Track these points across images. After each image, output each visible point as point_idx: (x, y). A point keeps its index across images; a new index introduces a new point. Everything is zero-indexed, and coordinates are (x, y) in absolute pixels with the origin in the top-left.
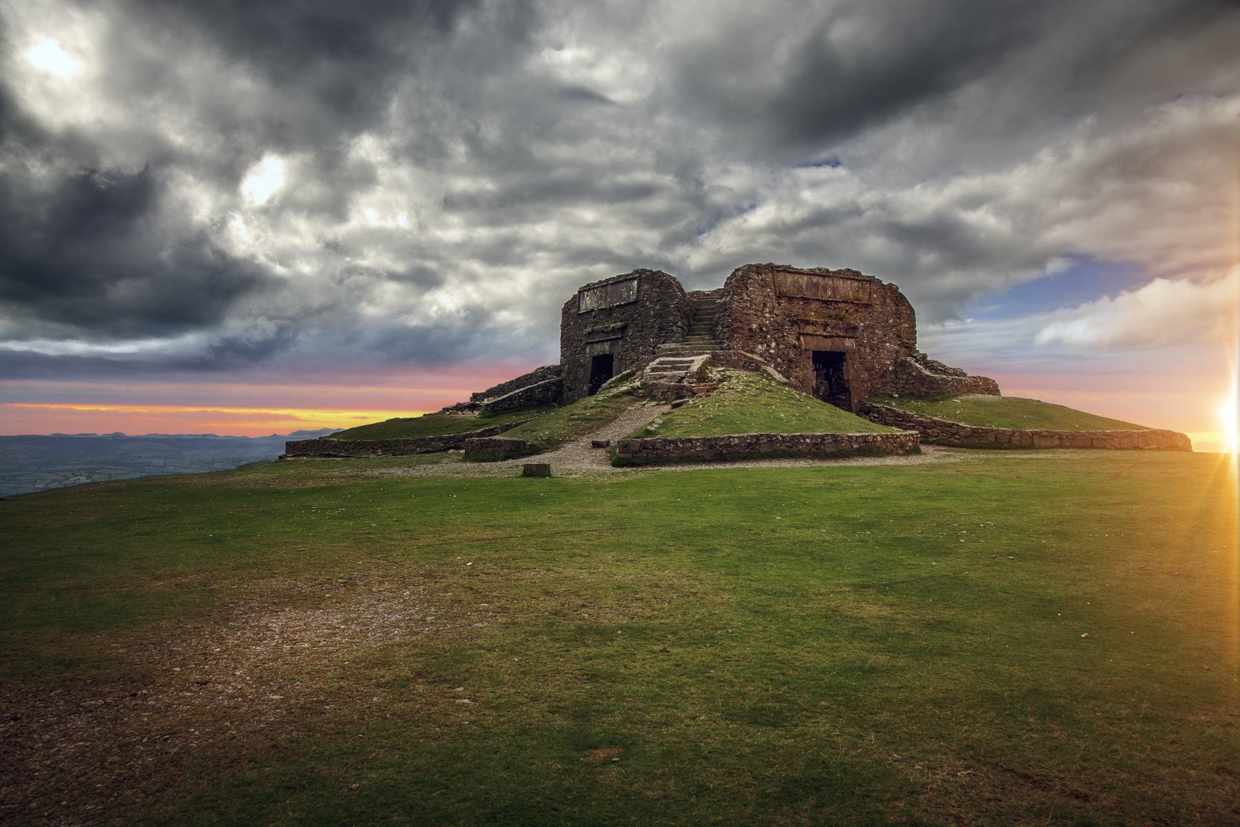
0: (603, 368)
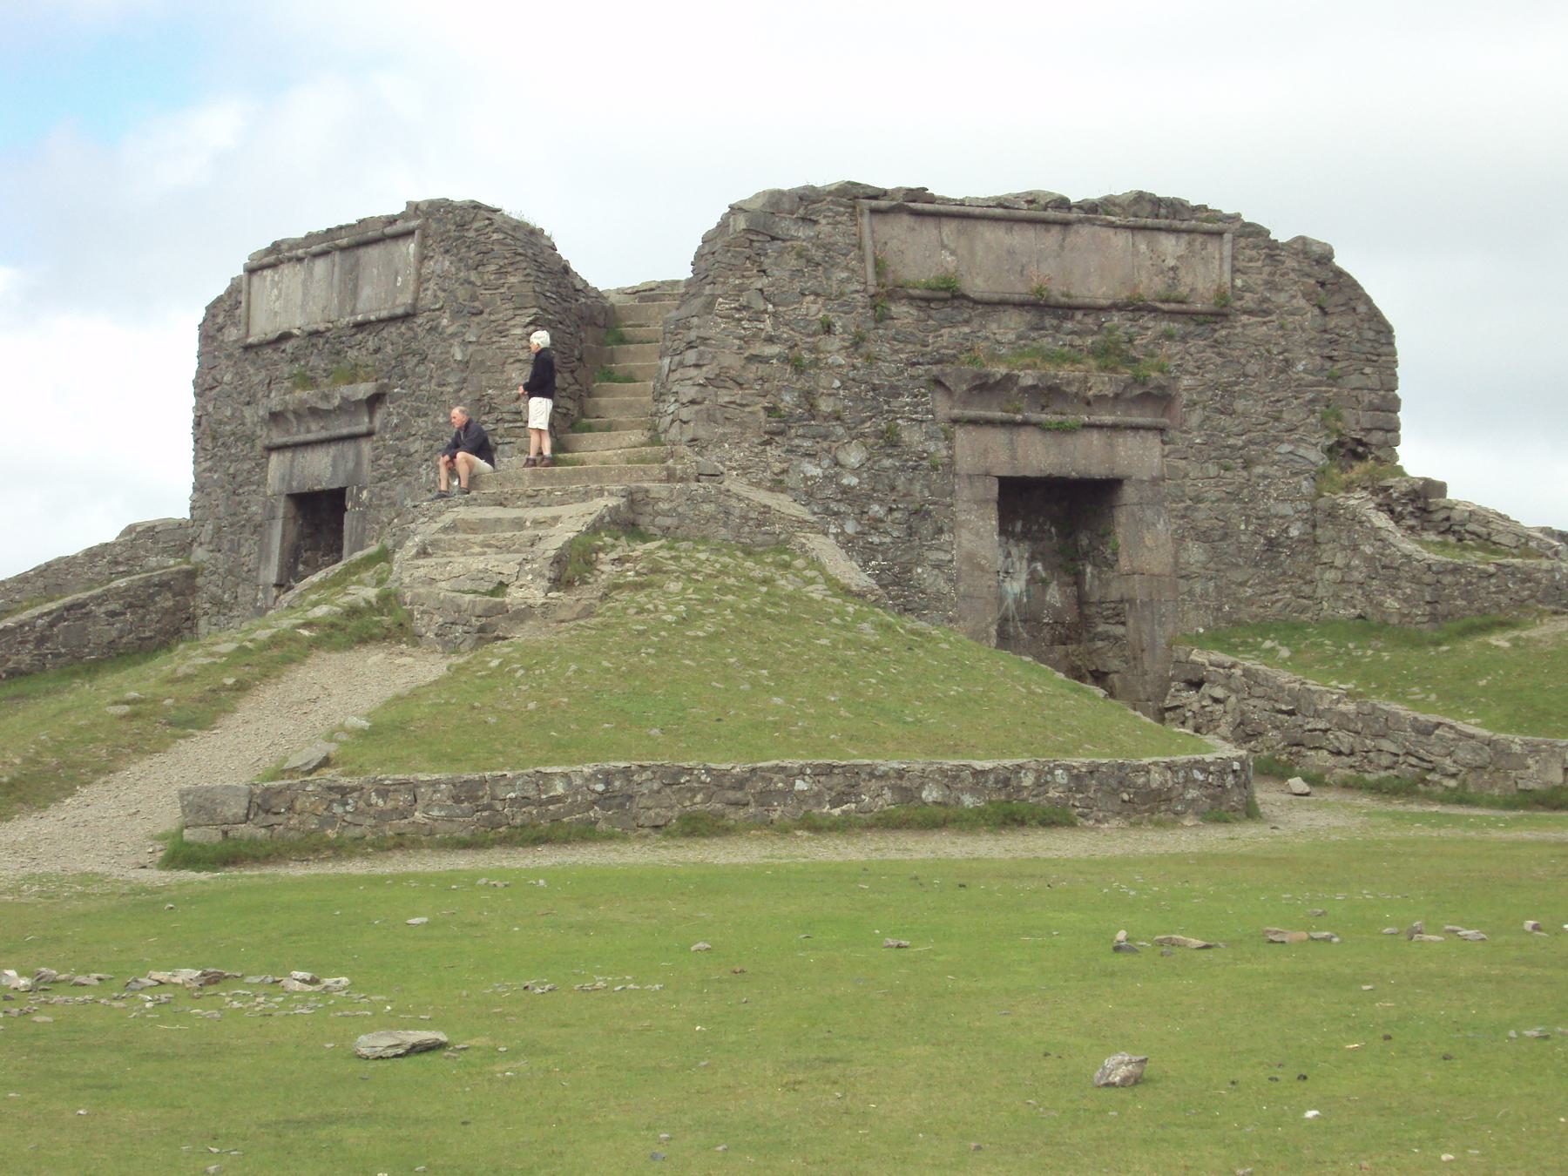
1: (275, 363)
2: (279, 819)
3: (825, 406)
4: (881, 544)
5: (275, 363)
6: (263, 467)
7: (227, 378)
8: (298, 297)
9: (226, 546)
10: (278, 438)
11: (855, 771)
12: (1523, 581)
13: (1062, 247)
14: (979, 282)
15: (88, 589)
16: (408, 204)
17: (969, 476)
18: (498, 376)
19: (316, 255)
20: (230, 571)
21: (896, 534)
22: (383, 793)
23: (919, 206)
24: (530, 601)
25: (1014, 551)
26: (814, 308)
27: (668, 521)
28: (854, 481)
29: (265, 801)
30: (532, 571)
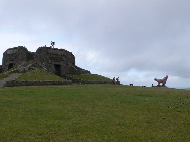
0: (11, 66)
3: (44, 59)
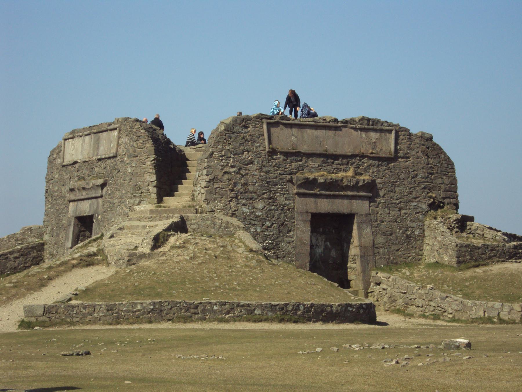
1: (72, 172)
2: (54, 315)
4: (269, 235)
5: (72, 172)
6: (67, 207)
7: (57, 176)
8: (80, 149)
9: (55, 234)
10: (73, 197)
11: (233, 304)
12: (492, 250)
13: (335, 135)
14: (305, 147)
15: (7, 249)
16: (116, 119)
17: (300, 212)
18: (142, 178)
19: (86, 135)
20: (56, 244)
21: (275, 232)
22: (85, 308)
23: (284, 121)
24: (145, 252)
25: (320, 238)
26: (247, 156)
27: (195, 227)
28: (260, 214)
29: (49, 310)
30: (146, 242)
